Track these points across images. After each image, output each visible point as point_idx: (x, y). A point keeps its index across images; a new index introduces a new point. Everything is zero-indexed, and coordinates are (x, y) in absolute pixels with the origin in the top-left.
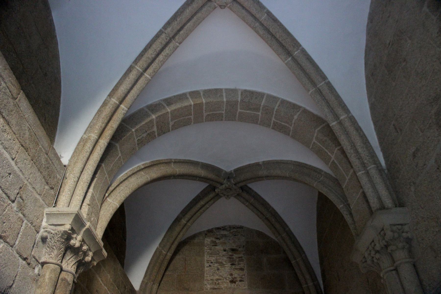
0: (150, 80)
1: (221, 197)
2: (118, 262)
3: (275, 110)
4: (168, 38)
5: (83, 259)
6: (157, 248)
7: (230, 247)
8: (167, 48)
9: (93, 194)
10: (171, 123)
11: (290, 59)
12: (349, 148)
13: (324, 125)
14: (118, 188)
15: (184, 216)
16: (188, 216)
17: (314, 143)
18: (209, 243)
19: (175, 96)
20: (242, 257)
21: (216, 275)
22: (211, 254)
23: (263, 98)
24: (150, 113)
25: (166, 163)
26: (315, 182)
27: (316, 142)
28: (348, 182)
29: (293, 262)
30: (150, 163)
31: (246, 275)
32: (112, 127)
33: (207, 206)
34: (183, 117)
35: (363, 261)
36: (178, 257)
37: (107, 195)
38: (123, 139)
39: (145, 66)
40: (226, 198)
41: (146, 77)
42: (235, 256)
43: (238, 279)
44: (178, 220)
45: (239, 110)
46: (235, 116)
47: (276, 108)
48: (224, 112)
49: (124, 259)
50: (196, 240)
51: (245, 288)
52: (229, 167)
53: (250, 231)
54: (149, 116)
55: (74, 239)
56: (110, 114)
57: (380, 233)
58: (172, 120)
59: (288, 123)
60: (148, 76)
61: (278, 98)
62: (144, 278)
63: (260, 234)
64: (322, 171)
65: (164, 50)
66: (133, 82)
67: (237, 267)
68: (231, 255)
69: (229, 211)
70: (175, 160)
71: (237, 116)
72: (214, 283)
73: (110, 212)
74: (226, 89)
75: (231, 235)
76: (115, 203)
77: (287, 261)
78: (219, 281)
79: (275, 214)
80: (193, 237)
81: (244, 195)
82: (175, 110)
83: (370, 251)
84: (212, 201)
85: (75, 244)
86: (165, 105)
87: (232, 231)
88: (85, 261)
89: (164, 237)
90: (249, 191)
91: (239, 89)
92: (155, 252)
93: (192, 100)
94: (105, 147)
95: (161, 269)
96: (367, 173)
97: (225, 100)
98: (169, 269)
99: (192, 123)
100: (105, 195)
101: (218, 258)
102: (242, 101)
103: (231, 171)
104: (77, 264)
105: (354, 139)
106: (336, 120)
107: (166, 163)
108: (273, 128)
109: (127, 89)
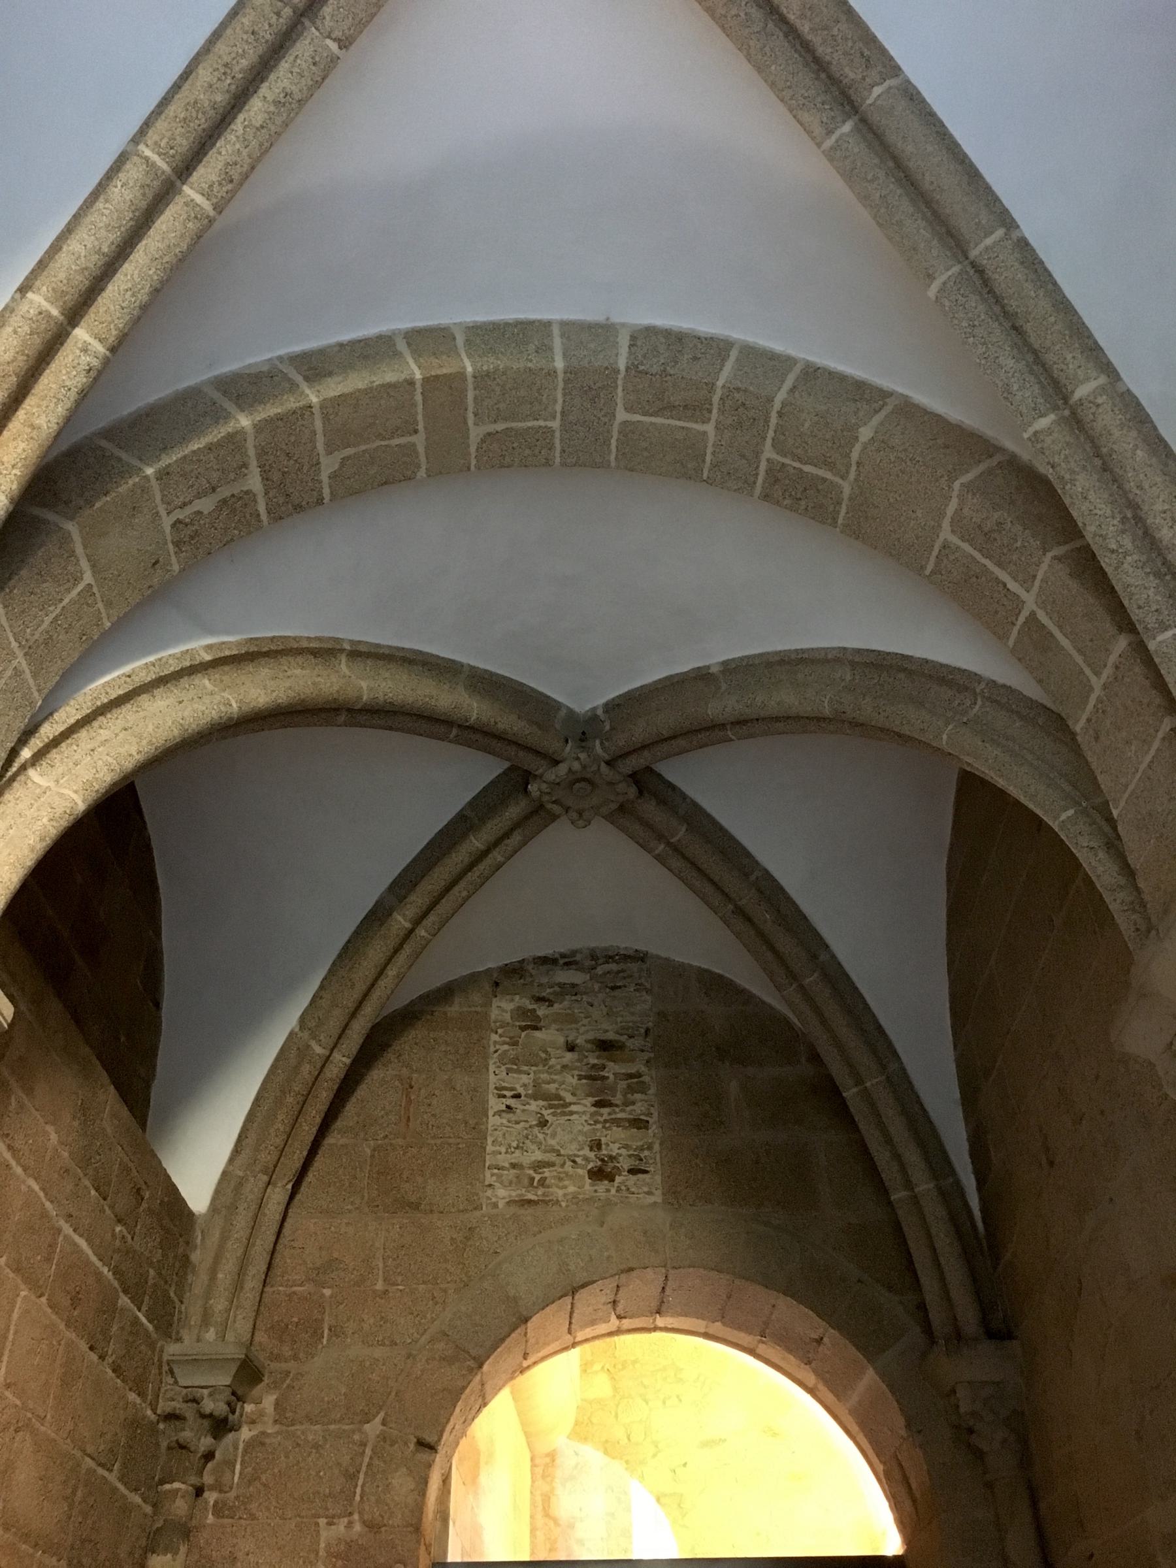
0: (211, 221)
1: (554, 817)
2: (105, 1078)
3: (777, 405)
4: (287, 12)
6: (292, 1034)
7: (591, 1036)
8: (284, 66)
10: (329, 465)
11: (847, 127)
12: (1112, 527)
13: (994, 462)
14: (83, 734)
15: (402, 899)
16: (417, 900)
17: (945, 546)
18: (507, 1017)
19: (341, 345)
21: (534, 1147)
22: (514, 1064)
25: (315, 653)
26: (947, 724)
27: (955, 540)
28: (1099, 700)
29: (850, 1093)
31: (657, 1147)
33: (497, 856)
36: (377, 1074)
37: (26, 754)
38: (98, 505)
39: (184, 144)
41: (190, 203)
42: (612, 1070)
43: (625, 1164)
44: (377, 916)
45: (621, 415)
46: (607, 443)
48: (555, 424)
50: (455, 1008)
51: (651, 1199)
52: (582, 694)
53: (676, 971)
54: (228, 417)
56: (22, 363)
58: (330, 450)
60: (199, 199)
62: (231, 1160)
63: (714, 984)
64: (977, 677)
65: (272, 77)
66: (127, 220)
67: (620, 1116)
68: (594, 1066)
69: (587, 885)
70: (352, 642)
71: (614, 442)
72: (526, 1181)
73: (38, 826)
74: (564, 324)
75: (596, 986)
76: (66, 791)
78: (547, 1172)
79: (770, 891)
80: (446, 993)
81: (649, 808)
84: (516, 837)
86: (299, 379)
87: (599, 971)
89: (322, 987)
91: (623, 325)
92: (283, 1051)
93: (416, 361)
95: (308, 1127)
97: (559, 364)
98: (339, 1124)
99: (422, 473)
100: (14, 753)
101: (544, 1076)
102: (633, 368)
103: (594, 709)
105: (1140, 487)
106: (1055, 408)
107: (315, 653)
108: (766, 497)
109: (99, 252)
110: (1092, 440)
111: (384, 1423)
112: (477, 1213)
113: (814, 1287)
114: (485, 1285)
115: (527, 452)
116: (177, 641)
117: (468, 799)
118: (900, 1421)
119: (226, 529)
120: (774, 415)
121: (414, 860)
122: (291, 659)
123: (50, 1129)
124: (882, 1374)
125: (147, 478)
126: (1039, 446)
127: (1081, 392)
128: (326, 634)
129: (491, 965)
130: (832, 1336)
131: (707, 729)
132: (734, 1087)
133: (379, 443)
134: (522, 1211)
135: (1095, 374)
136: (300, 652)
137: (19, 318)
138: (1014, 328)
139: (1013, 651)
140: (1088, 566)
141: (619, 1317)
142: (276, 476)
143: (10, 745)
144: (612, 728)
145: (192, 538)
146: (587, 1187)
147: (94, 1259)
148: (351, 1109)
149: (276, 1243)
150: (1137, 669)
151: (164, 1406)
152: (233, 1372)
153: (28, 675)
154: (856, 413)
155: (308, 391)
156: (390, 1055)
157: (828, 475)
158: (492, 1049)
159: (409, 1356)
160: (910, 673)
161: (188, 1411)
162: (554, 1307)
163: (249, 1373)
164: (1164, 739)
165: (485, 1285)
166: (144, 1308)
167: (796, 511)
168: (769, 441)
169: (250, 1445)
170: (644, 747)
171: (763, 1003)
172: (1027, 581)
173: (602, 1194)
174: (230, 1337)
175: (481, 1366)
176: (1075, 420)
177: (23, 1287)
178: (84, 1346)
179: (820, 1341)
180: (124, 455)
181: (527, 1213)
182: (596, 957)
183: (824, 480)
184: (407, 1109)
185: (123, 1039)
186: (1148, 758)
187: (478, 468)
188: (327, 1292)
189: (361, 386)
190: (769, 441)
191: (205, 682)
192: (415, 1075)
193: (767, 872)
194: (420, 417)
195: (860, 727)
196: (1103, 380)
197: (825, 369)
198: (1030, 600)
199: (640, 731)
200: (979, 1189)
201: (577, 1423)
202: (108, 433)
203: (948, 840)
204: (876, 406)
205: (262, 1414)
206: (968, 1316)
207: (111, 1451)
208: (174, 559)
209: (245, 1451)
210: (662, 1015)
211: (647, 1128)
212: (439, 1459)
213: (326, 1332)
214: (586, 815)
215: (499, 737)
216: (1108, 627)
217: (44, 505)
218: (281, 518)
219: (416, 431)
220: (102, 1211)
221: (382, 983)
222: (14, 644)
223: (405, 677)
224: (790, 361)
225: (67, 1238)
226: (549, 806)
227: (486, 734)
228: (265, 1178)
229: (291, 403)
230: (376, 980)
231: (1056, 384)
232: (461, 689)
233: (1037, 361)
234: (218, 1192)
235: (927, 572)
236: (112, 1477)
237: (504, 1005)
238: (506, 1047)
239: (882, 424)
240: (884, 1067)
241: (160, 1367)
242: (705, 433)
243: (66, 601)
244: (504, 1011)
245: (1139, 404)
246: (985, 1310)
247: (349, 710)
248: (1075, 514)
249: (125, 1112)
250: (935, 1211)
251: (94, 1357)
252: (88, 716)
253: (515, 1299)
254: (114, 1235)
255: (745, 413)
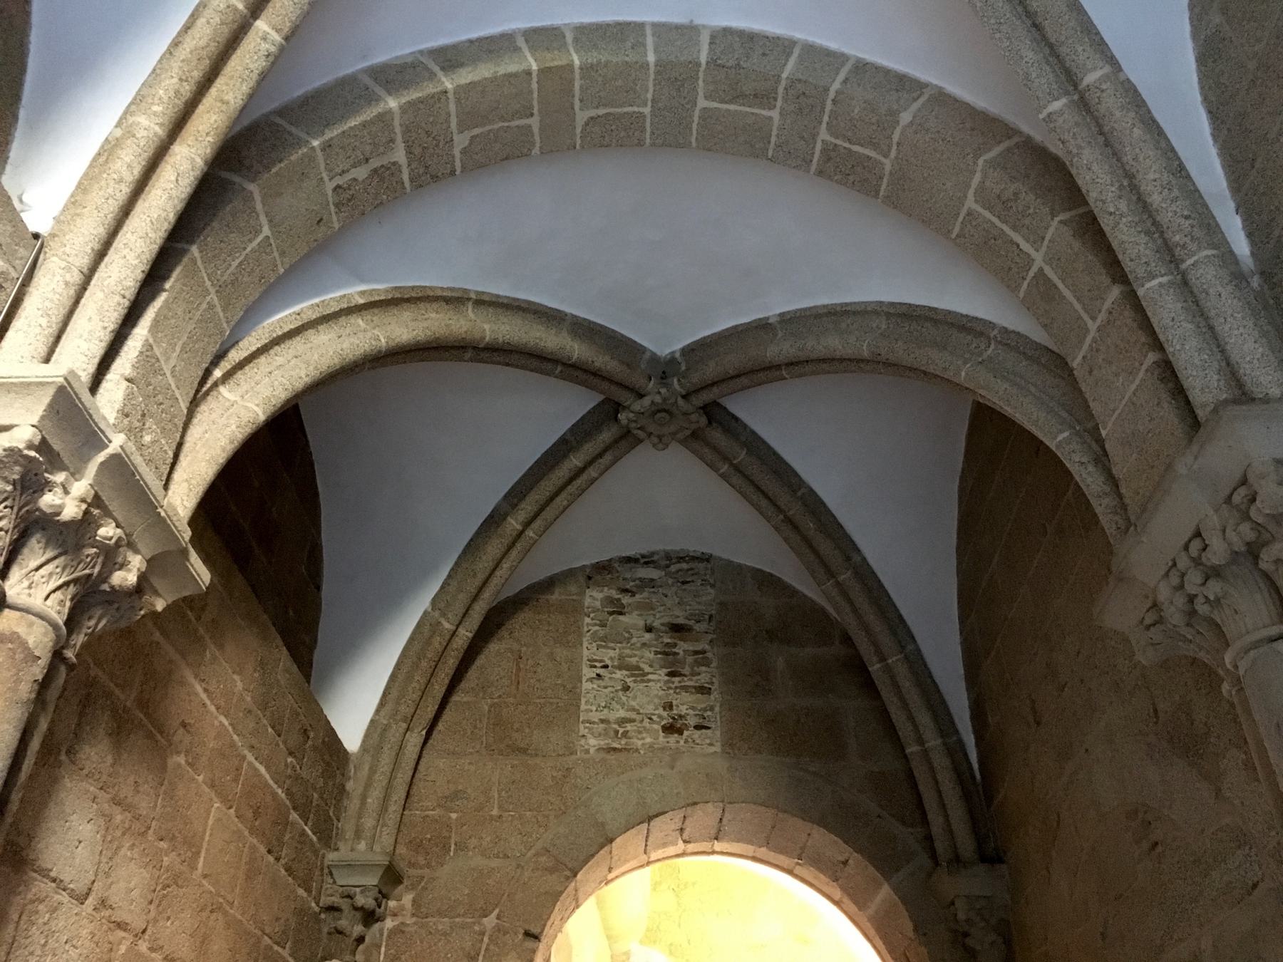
2: (279, 641)
3: (832, 95)
5: (104, 576)
6: (425, 613)
7: (666, 620)
9: (148, 347)
10: (461, 141)
12: (1111, 193)
14: (262, 360)
15: (514, 506)
17: (969, 214)
18: (598, 604)
19: (471, 41)
20: (704, 652)
22: (603, 642)
23: (789, 55)
24: (379, 91)
25: (447, 300)
26: (965, 363)
28: (1094, 340)
29: (875, 668)
30: (387, 291)
31: (717, 709)
32: (222, 101)
33: (592, 472)
34: (502, 119)
35: (1148, 621)
36: (493, 647)
37: (218, 373)
38: (274, 170)
40: (654, 445)
42: (682, 647)
43: (692, 721)
44: (493, 521)
45: (702, 103)
47: (836, 86)
48: (647, 110)
49: (311, 648)
50: (556, 596)
51: (712, 749)
52: (665, 341)
53: (738, 570)
54: (378, 99)
55: (59, 490)
57: (1229, 499)
59: (875, 146)
61: (843, 55)
62: (378, 711)
63: (766, 581)
64: (992, 325)
69: (665, 499)
70: (477, 293)
72: (612, 733)
73: (228, 431)
74: (654, 25)
76: (250, 405)
77: (857, 667)
78: (629, 727)
80: (548, 584)
81: (716, 435)
82: (472, 85)
83: (1183, 575)
84: (608, 457)
85: (61, 507)
86: (436, 69)
87: (673, 568)
88: (112, 587)
89: (449, 576)
90: (732, 426)
91: (704, 26)
92: (419, 626)
93: (533, 55)
94: (198, 173)
95: (440, 684)
96: (1184, 284)
97: (651, 58)
99: (536, 151)
100: (208, 373)
101: (628, 651)
102: (712, 62)
103: (673, 352)
104: (72, 589)
106: (1067, 93)
107: (447, 300)
108: (820, 173)
110: (1096, 119)
111: (498, 918)
112: (574, 757)
113: (843, 821)
114: (579, 813)
115: (623, 134)
116: (339, 287)
117: (569, 426)
118: (908, 926)
119: (377, 194)
120: (829, 102)
121: (524, 475)
122: (428, 305)
123: (236, 677)
124: (896, 890)
125: (313, 148)
126: (1052, 125)
127: (1090, 78)
128: (457, 285)
129: (587, 563)
130: (855, 858)
131: (764, 369)
132: (780, 663)
133: (501, 124)
134: (608, 757)
135: (1101, 64)
136: (436, 299)
137: (211, 11)
138: (1035, 25)
139: (1023, 301)
140: (1091, 230)
141: (685, 841)
142: (417, 151)
143: (205, 366)
144: (687, 369)
145: (349, 200)
146: (661, 739)
147: (271, 782)
148: (472, 673)
149: (413, 776)
150: (1126, 313)
151: (325, 900)
152: (380, 873)
153: (219, 309)
154: (897, 101)
155: (444, 79)
156: (504, 632)
157: (872, 154)
158: (586, 629)
159: (518, 866)
160: (935, 322)
161: (345, 904)
162: (633, 831)
163: (392, 876)
164: (1147, 371)
165: (579, 813)
166: (310, 823)
167: (845, 184)
168: (824, 125)
169: (394, 932)
170: (713, 384)
171: (805, 596)
172: (1037, 241)
173: (673, 745)
174: (377, 848)
175: (575, 876)
176: (1084, 104)
177: (215, 799)
178: (263, 849)
179: (845, 863)
180: (293, 130)
181: (611, 757)
182: (671, 558)
183: (869, 158)
184: (517, 675)
185: (291, 613)
186: (1133, 387)
187: (583, 147)
188: (454, 816)
189: (487, 74)
190: (824, 125)
191: (359, 321)
192: (524, 649)
193: (812, 490)
194: (535, 103)
195: (891, 366)
196: (1107, 69)
197: (873, 64)
198: (1038, 258)
199: (711, 370)
200: (977, 745)
201: (648, 930)
202: (282, 112)
203: (960, 465)
204: (915, 95)
205: (402, 908)
206: (966, 844)
207: (284, 932)
208: (335, 218)
209: (389, 937)
210: (723, 605)
211: (709, 694)
212: (542, 946)
213: (453, 847)
214: (665, 439)
215: (596, 374)
216: (1105, 280)
217: (231, 170)
218: (421, 186)
219: (532, 115)
220: (277, 745)
221: (498, 573)
222: (208, 283)
223: (519, 322)
224: (843, 58)
225: (250, 764)
226: (635, 432)
227: (585, 371)
228: (404, 725)
229: (430, 89)
230: (494, 570)
231: (1068, 73)
232: (565, 334)
233: (1052, 52)
234: (367, 736)
235: (953, 236)
236: (285, 953)
237: (595, 594)
238: (597, 628)
239: (919, 110)
240: (903, 648)
241: (322, 869)
242: (770, 118)
243: (249, 249)
244: (594, 599)
245: (1136, 91)
246: (980, 840)
247: (474, 348)
248: (1080, 182)
249: (295, 668)
250: (941, 762)
251: (271, 859)
252: (266, 345)
253: (603, 824)
254: (286, 765)
255: (806, 100)
